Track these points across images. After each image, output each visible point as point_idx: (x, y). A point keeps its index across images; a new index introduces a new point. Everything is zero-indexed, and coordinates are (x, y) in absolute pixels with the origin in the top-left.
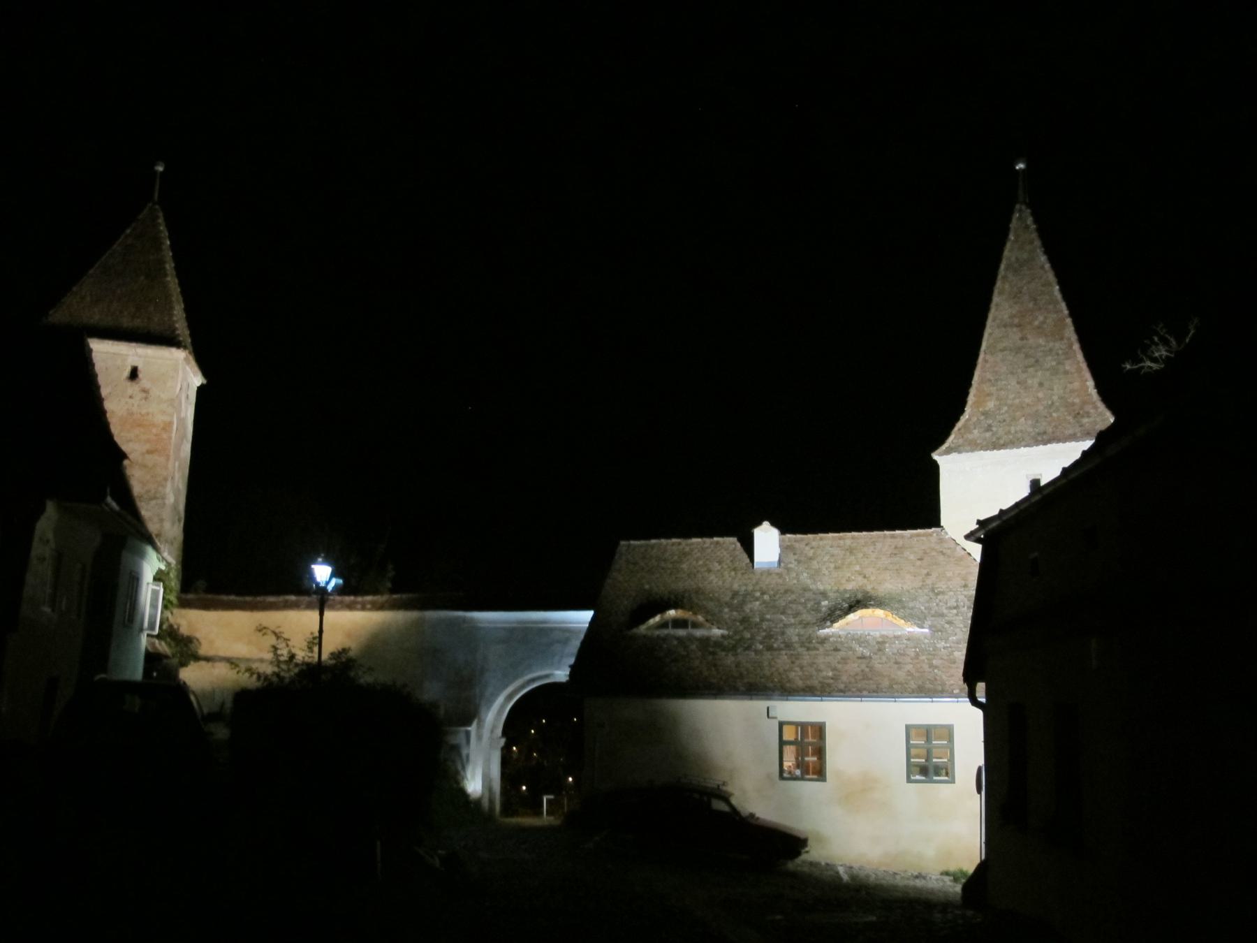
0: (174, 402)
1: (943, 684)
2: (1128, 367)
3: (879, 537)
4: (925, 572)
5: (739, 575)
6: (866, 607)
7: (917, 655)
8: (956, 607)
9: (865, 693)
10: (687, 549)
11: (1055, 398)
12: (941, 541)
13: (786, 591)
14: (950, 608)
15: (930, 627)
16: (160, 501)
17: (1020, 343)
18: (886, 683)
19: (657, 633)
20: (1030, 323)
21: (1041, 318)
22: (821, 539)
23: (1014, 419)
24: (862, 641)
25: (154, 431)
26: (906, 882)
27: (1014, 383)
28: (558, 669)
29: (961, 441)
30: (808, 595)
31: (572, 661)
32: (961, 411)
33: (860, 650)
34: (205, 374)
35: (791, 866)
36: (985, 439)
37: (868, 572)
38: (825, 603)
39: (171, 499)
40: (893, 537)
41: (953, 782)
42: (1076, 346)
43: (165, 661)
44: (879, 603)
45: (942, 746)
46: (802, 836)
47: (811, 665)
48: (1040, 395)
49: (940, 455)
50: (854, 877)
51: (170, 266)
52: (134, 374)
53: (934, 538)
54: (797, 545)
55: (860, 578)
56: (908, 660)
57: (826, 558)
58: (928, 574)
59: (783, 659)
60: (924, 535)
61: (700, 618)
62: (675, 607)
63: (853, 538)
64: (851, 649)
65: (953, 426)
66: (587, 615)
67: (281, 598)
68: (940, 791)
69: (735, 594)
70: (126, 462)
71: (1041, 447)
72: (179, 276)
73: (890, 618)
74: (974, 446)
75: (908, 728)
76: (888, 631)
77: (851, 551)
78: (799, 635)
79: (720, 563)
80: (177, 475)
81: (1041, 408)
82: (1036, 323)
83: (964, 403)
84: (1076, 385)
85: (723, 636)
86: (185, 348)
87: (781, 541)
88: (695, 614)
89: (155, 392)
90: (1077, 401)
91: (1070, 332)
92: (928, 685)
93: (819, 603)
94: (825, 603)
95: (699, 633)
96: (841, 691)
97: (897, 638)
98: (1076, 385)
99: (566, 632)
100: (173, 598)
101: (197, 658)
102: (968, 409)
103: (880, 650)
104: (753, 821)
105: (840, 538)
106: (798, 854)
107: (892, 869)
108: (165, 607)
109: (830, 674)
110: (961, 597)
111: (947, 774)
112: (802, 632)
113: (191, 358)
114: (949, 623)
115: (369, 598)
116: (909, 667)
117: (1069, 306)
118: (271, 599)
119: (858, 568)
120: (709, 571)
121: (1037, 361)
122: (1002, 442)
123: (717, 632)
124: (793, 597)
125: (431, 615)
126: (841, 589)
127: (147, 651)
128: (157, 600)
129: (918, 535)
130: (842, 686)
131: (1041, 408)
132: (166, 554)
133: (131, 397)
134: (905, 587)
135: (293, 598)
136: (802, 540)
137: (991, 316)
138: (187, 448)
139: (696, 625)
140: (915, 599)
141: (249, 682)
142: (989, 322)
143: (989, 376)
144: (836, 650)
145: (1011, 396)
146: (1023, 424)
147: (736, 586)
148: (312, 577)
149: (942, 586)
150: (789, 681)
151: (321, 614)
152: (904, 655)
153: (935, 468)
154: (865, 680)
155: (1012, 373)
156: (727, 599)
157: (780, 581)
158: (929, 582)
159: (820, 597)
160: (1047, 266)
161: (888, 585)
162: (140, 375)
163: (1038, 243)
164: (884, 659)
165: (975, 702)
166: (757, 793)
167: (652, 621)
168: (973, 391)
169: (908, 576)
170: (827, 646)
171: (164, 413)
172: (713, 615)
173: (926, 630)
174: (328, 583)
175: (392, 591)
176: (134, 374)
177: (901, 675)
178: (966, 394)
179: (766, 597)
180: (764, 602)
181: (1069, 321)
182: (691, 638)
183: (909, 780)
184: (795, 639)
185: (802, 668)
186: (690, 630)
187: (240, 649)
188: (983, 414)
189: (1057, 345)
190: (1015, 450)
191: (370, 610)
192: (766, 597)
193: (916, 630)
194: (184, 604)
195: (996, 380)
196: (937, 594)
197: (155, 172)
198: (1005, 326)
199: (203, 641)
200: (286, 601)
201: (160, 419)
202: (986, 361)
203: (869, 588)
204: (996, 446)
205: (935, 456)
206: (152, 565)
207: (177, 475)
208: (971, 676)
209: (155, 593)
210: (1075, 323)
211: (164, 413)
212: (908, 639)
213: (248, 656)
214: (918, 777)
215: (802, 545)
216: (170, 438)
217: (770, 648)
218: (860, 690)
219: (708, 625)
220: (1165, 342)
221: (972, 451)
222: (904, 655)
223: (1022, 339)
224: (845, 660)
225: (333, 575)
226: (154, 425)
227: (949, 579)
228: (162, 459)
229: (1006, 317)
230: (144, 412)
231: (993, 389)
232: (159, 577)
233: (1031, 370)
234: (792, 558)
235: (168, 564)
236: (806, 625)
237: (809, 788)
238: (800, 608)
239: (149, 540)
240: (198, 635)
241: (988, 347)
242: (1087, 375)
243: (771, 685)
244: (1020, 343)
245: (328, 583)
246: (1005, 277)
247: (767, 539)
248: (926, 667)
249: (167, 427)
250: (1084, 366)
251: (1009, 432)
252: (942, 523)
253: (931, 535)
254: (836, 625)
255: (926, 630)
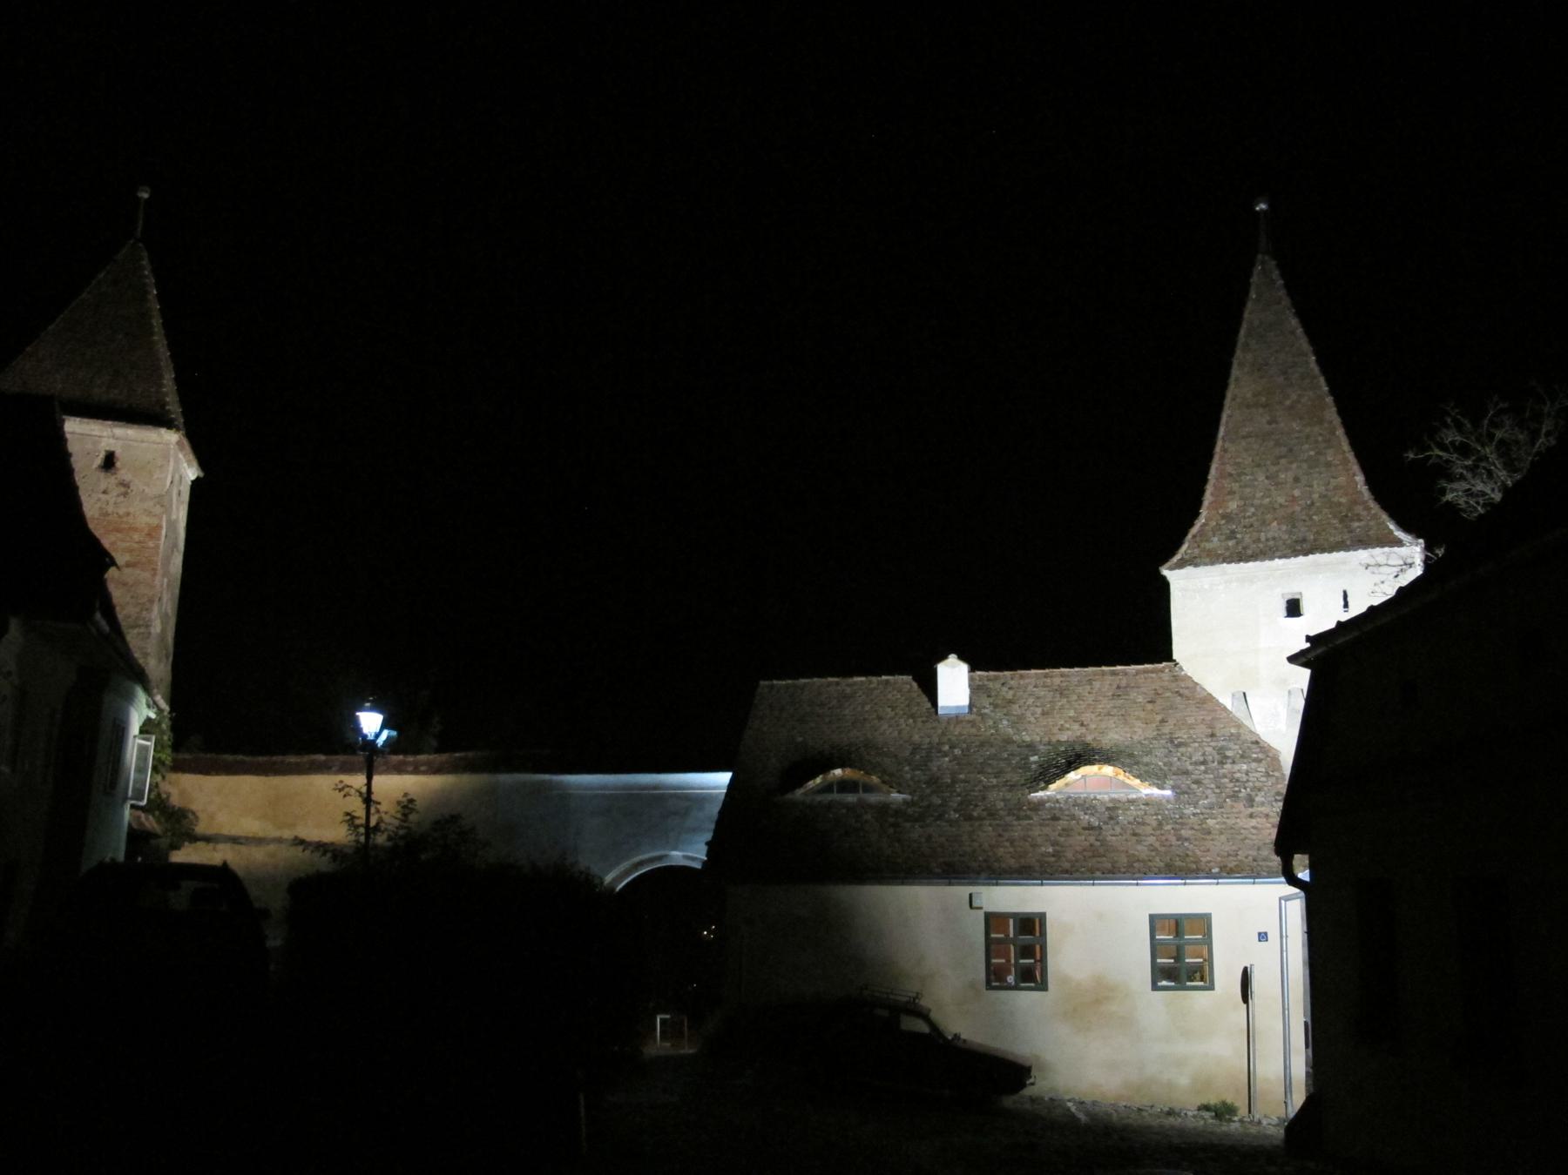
0: (162, 500)
1: (1197, 862)
2: (1411, 456)
3: (1095, 674)
4: (1159, 718)
5: (920, 724)
6: (1091, 763)
7: (1160, 824)
8: (1204, 763)
9: (1098, 874)
10: (848, 690)
11: (1316, 496)
12: (1176, 678)
13: (982, 744)
14: (1196, 763)
15: (1173, 788)
16: (142, 630)
17: (1267, 427)
18: (1123, 860)
19: (819, 798)
20: (1281, 403)
21: (1294, 397)
22: (1022, 677)
23: (1264, 523)
24: (1087, 805)
25: (136, 537)
26: (1155, 1123)
27: (1261, 477)
28: (675, 849)
29: (1197, 551)
30: (1010, 748)
31: (708, 836)
32: (1196, 514)
33: (1085, 818)
34: (202, 464)
35: (1008, 1101)
36: (1227, 549)
37: (1087, 717)
38: (1034, 758)
39: (157, 628)
40: (1114, 673)
41: (1211, 987)
42: (1340, 432)
43: (153, 842)
44: (1107, 758)
45: (1196, 942)
46: (1027, 1064)
47: (1025, 839)
48: (1297, 493)
49: (1171, 569)
50: (1092, 1116)
51: (157, 322)
52: (109, 462)
53: (1166, 676)
54: (991, 685)
55: (1076, 726)
56: (1148, 830)
57: (1030, 701)
58: (1163, 721)
59: (987, 832)
60: (1152, 671)
61: (875, 779)
62: (842, 766)
63: (1062, 675)
64: (1073, 817)
65: (1185, 534)
66: (723, 778)
67: (306, 758)
68: (1197, 1000)
69: (916, 749)
70: (112, 573)
71: (1301, 559)
72: (167, 336)
73: (1121, 777)
74: (1214, 558)
75: (1151, 917)
76: (1120, 795)
77: (1062, 692)
78: (1004, 800)
79: (893, 708)
80: (165, 597)
81: (1298, 508)
82: (1288, 403)
83: (1199, 504)
84: (1342, 480)
85: (905, 802)
86: (178, 429)
87: (971, 679)
88: (867, 773)
89: (137, 485)
90: (1343, 500)
91: (1332, 414)
92: (1178, 863)
93: (1027, 758)
94: (1034, 758)
95: (873, 798)
96: (1067, 872)
97: (1132, 802)
98: (1342, 480)
99: (695, 800)
100: (167, 756)
101: (194, 838)
102: (1204, 512)
103: (1111, 818)
104: (960, 1044)
105: (1046, 676)
106: (1024, 1086)
107: (1138, 1102)
108: (155, 769)
109: (1051, 850)
110: (1209, 749)
111: (1202, 979)
112: (1009, 795)
113: (185, 442)
114: (1197, 782)
115: (422, 757)
116: (1152, 840)
117: (1329, 382)
118: (292, 759)
119: (1072, 713)
120: (880, 718)
121: (1291, 450)
122: (1249, 552)
123: (896, 797)
124: (993, 750)
125: (505, 778)
126: (1054, 740)
127: (131, 829)
128: (146, 759)
129: (1146, 671)
130: (1067, 865)
131: (1298, 508)
132: (158, 698)
133: (105, 492)
134: (1136, 738)
135: (322, 757)
136: (996, 678)
137: (1229, 395)
138: (178, 560)
139: (868, 788)
140: (1149, 753)
141: (324, 864)
142: (1227, 402)
143: (1229, 469)
144: (1055, 818)
145: (1259, 495)
146: (1275, 529)
147: (916, 738)
148: (357, 729)
149: (1182, 735)
150: (998, 860)
151: (369, 779)
152: (1144, 824)
153: (1164, 586)
154: (1098, 854)
155: (1259, 466)
156: (907, 753)
157: (974, 731)
158: (1166, 730)
159: (1025, 751)
160: (1300, 331)
161: (1113, 735)
162: (118, 464)
163: (1286, 301)
164: (1118, 830)
165: (1292, 880)
166: (959, 1006)
167: (811, 784)
168: (1209, 489)
169: (1138, 724)
170: (1044, 814)
171: (149, 513)
172: (891, 775)
173: (1168, 793)
174: (377, 735)
175: (438, 751)
176: (109, 462)
177: (1141, 850)
178: (1201, 493)
179: (957, 752)
180: (955, 758)
181: (1329, 400)
182: (863, 805)
183: (1155, 987)
184: (1001, 805)
185: (1012, 842)
186: (862, 795)
187: (250, 826)
188: (1224, 517)
189: (1316, 429)
190: (1267, 563)
191: (424, 773)
192: (957, 752)
193: (1155, 791)
194: (178, 767)
195: (1239, 475)
196: (1180, 745)
197: (139, 199)
198: (1248, 407)
199: (200, 814)
200: (313, 762)
201: (143, 521)
202: (1225, 450)
203: (1089, 738)
204: (1241, 557)
205: (1165, 572)
206: (140, 712)
207: (165, 597)
208: (1286, 845)
209: (143, 750)
210: (1337, 402)
211: (149, 513)
212: (1147, 804)
213: (261, 834)
214: (1164, 983)
215: (998, 685)
216: (157, 547)
217: (969, 818)
218: (1092, 871)
219: (885, 788)
220: (1459, 427)
221: (1212, 564)
222: (1144, 824)
223: (1269, 423)
224: (1067, 832)
225: (384, 726)
226: (135, 530)
227: (1191, 727)
228: (147, 575)
229: (1249, 395)
230: (122, 511)
231: (1235, 486)
232: (147, 728)
233: (1283, 461)
234: (986, 701)
235: (160, 711)
236: (1012, 787)
237: (1026, 999)
238: (1002, 764)
239: (140, 676)
240: (193, 807)
241: (1227, 433)
242: (1356, 468)
243: (974, 865)
244: (1267, 427)
245: (377, 735)
246: (1247, 345)
247: (954, 682)
248: (1173, 839)
249: (153, 533)
250: (1351, 456)
251: (1259, 540)
252: (1175, 657)
253: (1162, 671)
254: (1052, 787)
255: (1168, 793)
